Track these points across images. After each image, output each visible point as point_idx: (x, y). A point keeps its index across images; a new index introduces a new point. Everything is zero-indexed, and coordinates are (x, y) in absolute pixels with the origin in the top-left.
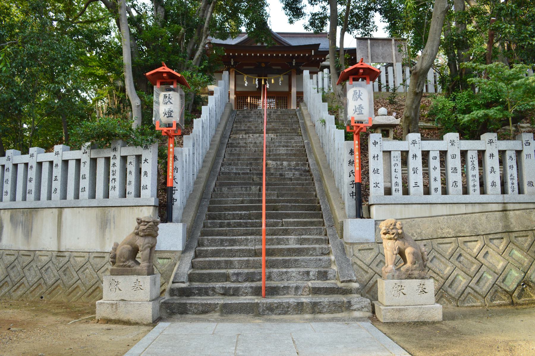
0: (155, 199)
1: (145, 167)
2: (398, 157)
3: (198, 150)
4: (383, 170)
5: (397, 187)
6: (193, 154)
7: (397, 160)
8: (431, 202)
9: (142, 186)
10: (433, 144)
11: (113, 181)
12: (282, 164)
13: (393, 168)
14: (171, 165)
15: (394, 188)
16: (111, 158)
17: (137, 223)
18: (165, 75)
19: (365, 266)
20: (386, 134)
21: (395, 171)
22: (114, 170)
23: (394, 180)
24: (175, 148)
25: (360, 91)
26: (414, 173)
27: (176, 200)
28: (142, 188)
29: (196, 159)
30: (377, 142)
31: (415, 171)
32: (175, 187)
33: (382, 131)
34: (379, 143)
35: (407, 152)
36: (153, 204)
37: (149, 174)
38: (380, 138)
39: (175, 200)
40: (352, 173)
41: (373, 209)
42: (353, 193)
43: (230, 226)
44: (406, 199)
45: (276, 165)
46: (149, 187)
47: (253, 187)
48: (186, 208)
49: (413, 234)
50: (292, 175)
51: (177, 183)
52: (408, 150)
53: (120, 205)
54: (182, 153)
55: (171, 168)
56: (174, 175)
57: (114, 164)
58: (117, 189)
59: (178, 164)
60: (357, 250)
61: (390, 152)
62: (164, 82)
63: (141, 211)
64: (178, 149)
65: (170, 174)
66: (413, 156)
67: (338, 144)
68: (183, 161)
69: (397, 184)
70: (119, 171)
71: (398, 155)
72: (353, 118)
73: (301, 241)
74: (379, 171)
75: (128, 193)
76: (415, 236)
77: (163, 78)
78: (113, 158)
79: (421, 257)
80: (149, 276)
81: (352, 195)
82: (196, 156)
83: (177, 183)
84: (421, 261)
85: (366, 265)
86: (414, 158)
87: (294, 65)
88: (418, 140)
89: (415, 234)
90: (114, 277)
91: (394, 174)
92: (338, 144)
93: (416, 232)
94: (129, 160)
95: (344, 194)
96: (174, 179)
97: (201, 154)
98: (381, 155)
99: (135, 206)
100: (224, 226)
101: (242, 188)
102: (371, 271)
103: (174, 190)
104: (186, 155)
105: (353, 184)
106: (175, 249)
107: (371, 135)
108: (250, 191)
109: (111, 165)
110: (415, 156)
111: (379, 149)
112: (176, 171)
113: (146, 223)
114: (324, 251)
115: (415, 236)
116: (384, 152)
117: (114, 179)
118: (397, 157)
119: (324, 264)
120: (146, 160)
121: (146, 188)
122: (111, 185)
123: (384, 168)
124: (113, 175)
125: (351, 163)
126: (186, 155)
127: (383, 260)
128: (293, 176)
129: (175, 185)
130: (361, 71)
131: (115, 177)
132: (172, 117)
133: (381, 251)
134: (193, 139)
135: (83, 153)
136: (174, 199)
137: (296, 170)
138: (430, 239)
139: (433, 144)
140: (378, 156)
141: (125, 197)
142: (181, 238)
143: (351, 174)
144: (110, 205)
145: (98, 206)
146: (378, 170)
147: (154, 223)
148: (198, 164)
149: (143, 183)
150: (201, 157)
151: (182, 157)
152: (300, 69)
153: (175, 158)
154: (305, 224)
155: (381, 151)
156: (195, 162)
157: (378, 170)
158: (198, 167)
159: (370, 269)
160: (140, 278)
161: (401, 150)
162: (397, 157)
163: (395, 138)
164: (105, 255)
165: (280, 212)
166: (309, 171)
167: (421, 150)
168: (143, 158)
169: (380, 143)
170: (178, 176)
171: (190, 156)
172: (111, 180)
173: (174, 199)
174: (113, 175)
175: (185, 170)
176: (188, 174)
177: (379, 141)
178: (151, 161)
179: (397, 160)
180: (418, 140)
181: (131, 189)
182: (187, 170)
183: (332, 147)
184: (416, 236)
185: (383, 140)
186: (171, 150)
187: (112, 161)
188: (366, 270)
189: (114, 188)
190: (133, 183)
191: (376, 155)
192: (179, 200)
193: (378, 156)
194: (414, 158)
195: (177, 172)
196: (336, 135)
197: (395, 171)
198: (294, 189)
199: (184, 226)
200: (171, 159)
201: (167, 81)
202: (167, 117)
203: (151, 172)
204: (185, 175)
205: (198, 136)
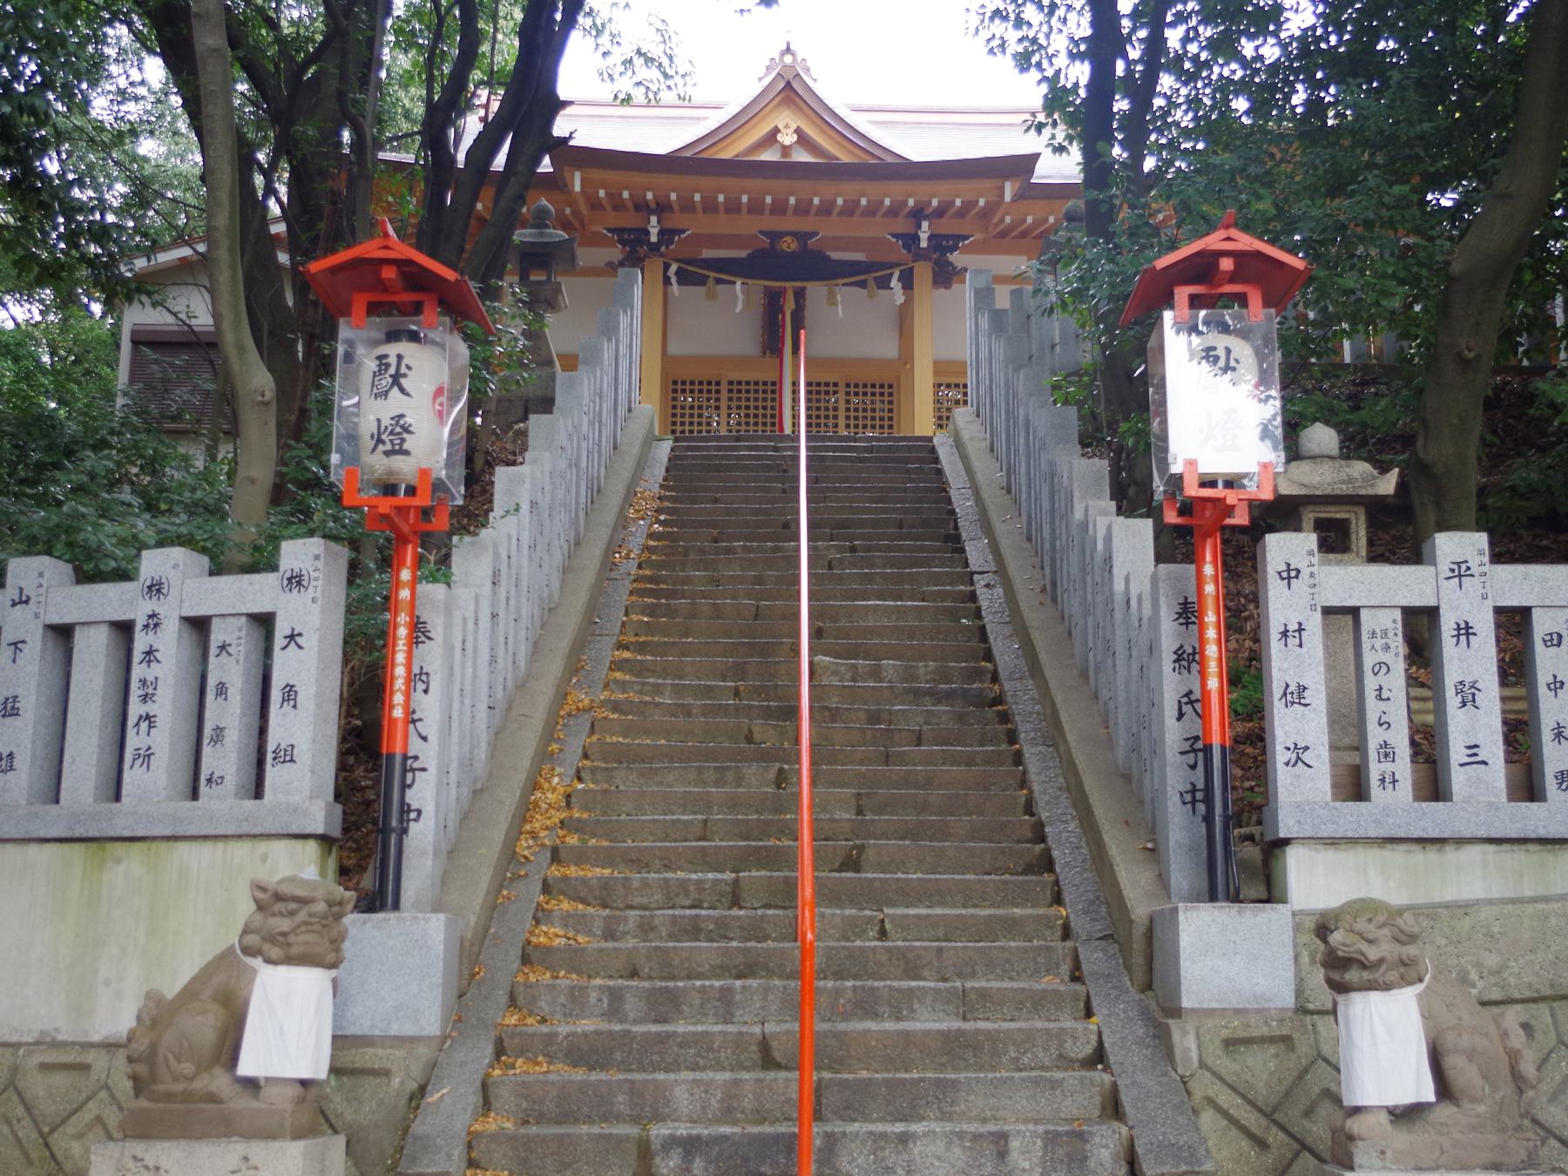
0: (327, 804)
1: (287, 667)
2: (1390, 635)
3: (512, 602)
4: (1323, 688)
5: (1387, 767)
6: (494, 616)
7: (1387, 648)
8: (1542, 833)
9: (271, 747)
10: (1546, 580)
11: (144, 725)
12: (876, 674)
13: (1371, 684)
14: (400, 658)
15: (1375, 770)
16: (138, 627)
17: (253, 907)
18: (389, 273)
19: (1256, 1114)
20: (1333, 540)
21: (1379, 698)
22: (150, 679)
23: (1375, 736)
24: (424, 588)
25: (1228, 351)
26: (1464, 704)
27: (419, 812)
28: (270, 756)
29: (502, 640)
30: (1298, 571)
31: (1469, 698)
32: (416, 758)
33: (1321, 526)
34: (1305, 573)
35: (1432, 613)
36: (320, 830)
37: (306, 696)
38: (1311, 553)
39: (413, 815)
40: (1191, 702)
41: (1294, 859)
42: (1194, 791)
43: (652, 936)
44: (1433, 818)
45: (849, 676)
46: (303, 753)
47: (751, 770)
48: (453, 853)
49: (1467, 973)
50: (920, 719)
51: (425, 739)
52: (1433, 603)
53: (168, 833)
54: (448, 610)
55: (400, 671)
56: (413, 706)
57: (149, 653)
58: (161, 760)
59: (431, 656)
60: (1217, 1041)
61: (1354, 612)
62: (380, 304)
63: (264, 858)
64: (433, 592)
65: (398, 698)
66: (1459, 628)
67: (1127, 579)
68: (452, 647)
69: (1387, 752)
70: (171, 681)
71: (1390, 625)
72: (1191, 463)
73: (966, 1005)
74: (1306, 694)
75: (209, 781)
76: (1473, 985)
77: (384, 287)
78: (146, 626)
79: (1506, 1071)
80: (301, 1144)
81: (1188, 798)
82: (501, 626)
83: (425, 739)
84: (1507, 1090)
85: (1261, 1111)
86: (1463, 638)
87: (924, 244)
88: (1478, 559)
89: (1474, 976)
90: (138, 1148)
91: (1373, 708)
92: (1127, 579)
93: (1478, 965)
94: (217, 635)
95: (1153, 801)
96: (414, 722)
97: (524, 622)
98: (1315, 623)
99: (240, 837)
100: (626, 933)
101: (700, 770)
102: (1281, 1136)
103: (413, 770)
104: (465, 620)
105: (1195, 751)
106: (408, 1029)
107: (1271, 539)
108: (739, 785)
109: (137, 656)
110: (1465, 631)
111: (1305, 601)
112: (421, 687)
113: (293, 906)
114: (1069, 1045)
115: (1473, 985)
116: (1328, 611)
117: (148, 717)
118: (1385, 633)
119: (1068, 1102)
120: (292, 637)
121: (287, 756)
122: (133, 741)
123: (1328, 688)
124: (145, 698)
125: (1188, 659)
126: (465, 620)
127: (1334, 1088)
128: (927, 723)
129: (415, 746)
130: (1226, 264)
131: (150, 708)
132: (407, 453)
133: (1326, 1050)
134: (496, 555)
135: (14, 604)
136: (409, 811)
137: (940, 698)
138: (1544, 999)
139: (1546, 580)
140: (1300, 630)
141: (195, 795)
142: (438, 979)
143: (1187, 709)
144: (126, 833)
145: (69, 834)
146: (1302, 689)
147: (330, 904)
148: (510, 666)
149: (276, 736)
150: (522, 635)
151: (448, 626)
152: (951, 264)
153: (418, 631)
154: (986, 930)
155: (1313, 608)
156: (501, 653)
157: (1302, 689)
158: (509, 676)
159: (1274, 1129)
160: (259, 1151)
161: (1405, 603)
162: (1385, 633)
163: (1374, 558)
164: (91, 1057)
165: (869, 875)
166: (999, 700)
167: (1490, 604)
168: (281, 629)
169: (1312, 575)
170: (429, 707)
171: (481, 623)
172: (132, 720)
173: (409, 811)
174: (145, 698)
175: (457, 687)
176: (468, 702)
177: (1306, 563)
178: (315, 642)
179: (1387, 648)
180: (1478, 559)
181: (225, 760)
182: (468, 688)
183: (1099, 598)
184: (1480, 984)
185: (1322, 563)
186: (405, 594)
187: (141, 642)
188: (1259, 1133)
189: (146, 756)
190: (233, 736)
191: (1293, 627)
192: (432, 814)
193: (1300, 630)
194: (1463, 638)
195: (426, 691)
196: (1115, 540)
197: (1379, 698)
198: (928, 783)
199: (449, 924)
200: (402, 632)
201: (396, 298)
202: (387, 453)
203: (313, 690)
204: (456, 706)
205: (514, 541)
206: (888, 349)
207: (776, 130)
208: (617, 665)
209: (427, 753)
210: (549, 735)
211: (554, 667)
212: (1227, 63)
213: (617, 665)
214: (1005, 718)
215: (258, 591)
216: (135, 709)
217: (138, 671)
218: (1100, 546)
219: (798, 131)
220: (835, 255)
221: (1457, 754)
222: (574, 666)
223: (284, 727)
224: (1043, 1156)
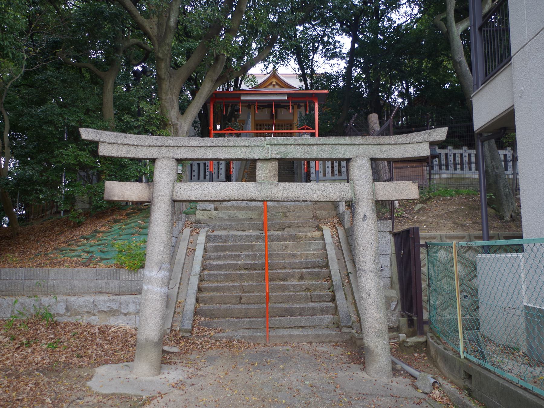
31: (328, 167)
137: (287, 170)
170: (234, 170)
206: (291, 118)
207: (272, 82)
208: (250, 167)
209: (234, 174)
210: (243, 175)
211: (243, 168)
212: (353, 73)
213: (250, 167)
214: (294, 172)
215: (461, 151)
216: (206, 171)
217: (206, 167)
218: (490, 134)
219: (276, 82)
220: (282, 104)
221: (327, 172)
222: (245, 168)
223: (221, 172)
224: (326, 295)
